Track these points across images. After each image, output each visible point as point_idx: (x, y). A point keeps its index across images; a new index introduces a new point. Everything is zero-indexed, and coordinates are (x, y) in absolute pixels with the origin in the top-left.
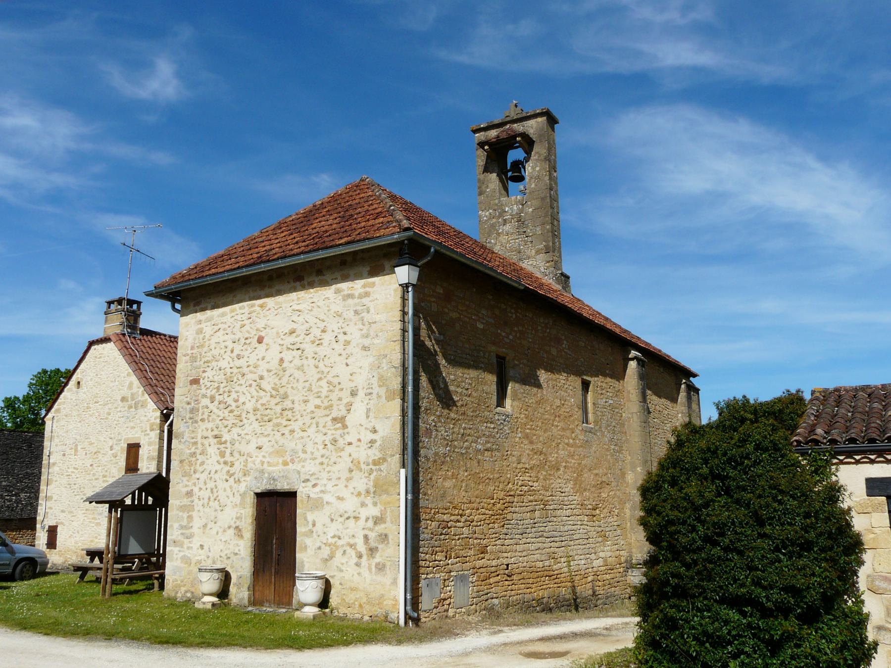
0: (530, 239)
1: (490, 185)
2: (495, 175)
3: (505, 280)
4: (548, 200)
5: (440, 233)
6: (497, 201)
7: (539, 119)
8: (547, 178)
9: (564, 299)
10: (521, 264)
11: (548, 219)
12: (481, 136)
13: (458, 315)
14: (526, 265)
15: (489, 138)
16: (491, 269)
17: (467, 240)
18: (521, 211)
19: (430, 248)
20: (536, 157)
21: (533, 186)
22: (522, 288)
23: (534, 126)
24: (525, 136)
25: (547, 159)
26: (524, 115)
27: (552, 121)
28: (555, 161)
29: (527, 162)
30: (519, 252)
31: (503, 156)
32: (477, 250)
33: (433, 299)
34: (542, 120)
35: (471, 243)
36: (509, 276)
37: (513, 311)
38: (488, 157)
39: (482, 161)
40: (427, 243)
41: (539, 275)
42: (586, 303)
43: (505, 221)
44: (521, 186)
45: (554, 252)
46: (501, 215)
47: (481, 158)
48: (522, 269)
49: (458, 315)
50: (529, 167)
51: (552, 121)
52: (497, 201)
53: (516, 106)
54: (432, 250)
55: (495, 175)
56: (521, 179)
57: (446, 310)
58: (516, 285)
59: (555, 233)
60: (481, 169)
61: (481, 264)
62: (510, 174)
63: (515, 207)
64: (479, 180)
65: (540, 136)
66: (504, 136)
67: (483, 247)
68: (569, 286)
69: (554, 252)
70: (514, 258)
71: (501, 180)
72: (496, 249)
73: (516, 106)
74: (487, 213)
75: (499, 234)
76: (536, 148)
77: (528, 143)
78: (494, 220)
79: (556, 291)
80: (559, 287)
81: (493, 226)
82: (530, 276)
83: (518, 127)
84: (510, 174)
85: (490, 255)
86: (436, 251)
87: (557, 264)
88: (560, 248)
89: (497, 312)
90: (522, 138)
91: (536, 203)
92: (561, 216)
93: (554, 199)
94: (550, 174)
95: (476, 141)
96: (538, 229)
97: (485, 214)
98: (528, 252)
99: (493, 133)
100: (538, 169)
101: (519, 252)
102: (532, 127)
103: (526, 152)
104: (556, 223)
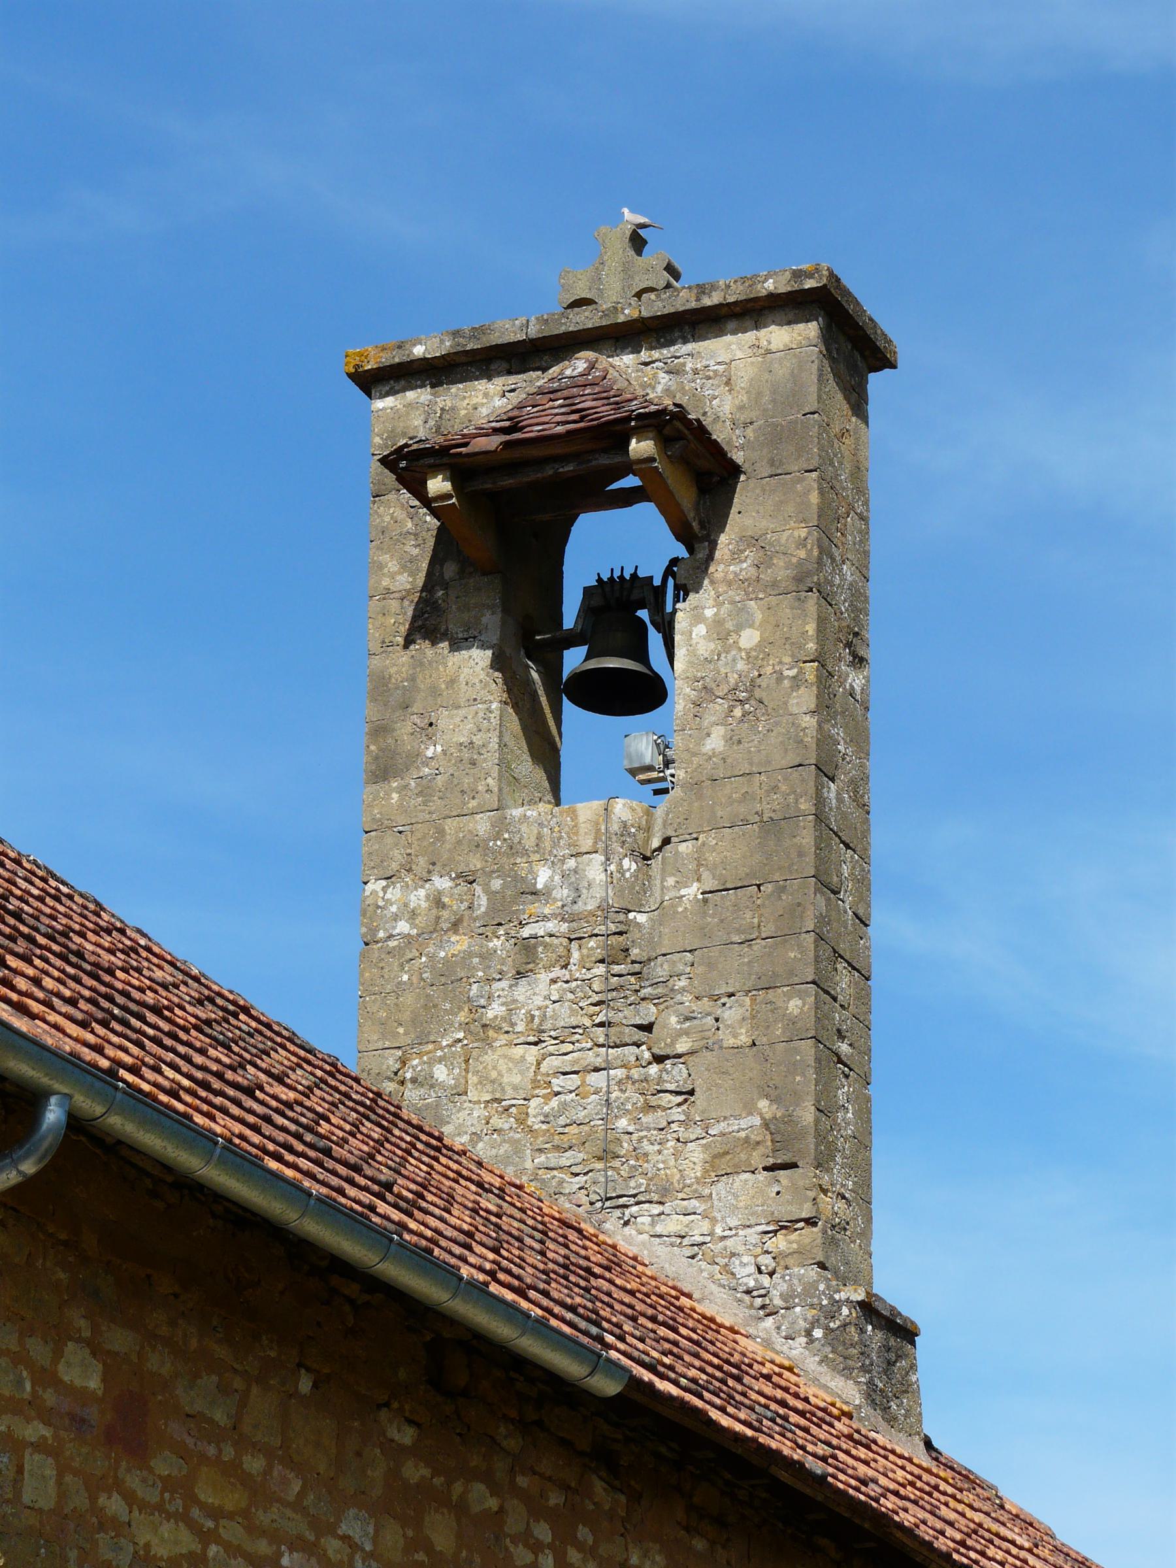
0: (676, 1075)
1: (445, 720)
2: (477, 660)
3: (502, 1330)
4: (806, 837)
5: (109, 1009)
6: (482, 825)
7: (777, 336)
8: (804, 700)
9: (875, 1476)
10: (613, 1230)
11: (800, 955)
12: (410, 414)
13: (187, 1542)
14: (648, 1240)
15: (456, 428)
16: (422, 1258)
17: (280, 1059)
18: (633, 896)
19: (35, 1099)
20: (745, 568)
21: (715, 742)
22: (610, 1387)
23: (745, 372)
24: (679, 430)
25: (813, 582)
26: (684, 300)
27: (855, 348)
28: (859, 599)
29: (683, 591)
30: (606, 1155)
31: (541, 541)
32: (335, 1126)
33: (35, 1431)
34: (794, 340)
35: (300, 1077)
36: (527, 1314)
37: (543, 1532)
38: (445, 547)
39: (407, 564)
40: (24, 1069)
41: (720, 1306)
42: (1017, 1497)
43: (528, 948)
44: (638, 738)
45: (821, 1164)
46: (502, 915)
47: (398, 542)
48: (615, 1261)
49: (187, 1542)
50: (696, 623)
51: (855, 348)
52: (482, 825)
53: (637, 242)
54: (53, 1115)
55: (477, 660)
56: (640, 694)
57: (114, 1505)
58: (570, 1367)
59: (838, 1050)
60: (400, 615)
61: (357, 1221)
62: (574, 659)
63: (595, 870)
64: (380, 686)
65: (775, 436)
66: (552, 421)
67: (378, 1109)
68: (907, 1389)
69: (821, 1164)
70: (571, 1196)
71: (519, 695)
72: (462, 1125)
73: (637, 242)
74: (419, 898)
75: (482, 1032)
76: (748, 512)
77: (699, 475)
78: (459, 943)
79: (824, 1416)
80: (846, 1391)
81: (450, 976)
82: (667, 1308)
83: (643, 377)
84: (574, 659)
85: (416, 1168)
86: (75, 1123)
87: (839, 1240)
88: (863, 1142)
89: (441, 1533)
90: (664, 441)
91: (729, 851)
92: (891, 931)
93: (841, 836)
94: (826, 676)
95: (379, 444)
96: (731, 1014)
97: (403, 902)
98: (661, 1159)
99: (484, 402)
100: (749, 638)
101: (606, 1155)
102: (732, 379)
103: (683, 533)
104: (844, 982)
